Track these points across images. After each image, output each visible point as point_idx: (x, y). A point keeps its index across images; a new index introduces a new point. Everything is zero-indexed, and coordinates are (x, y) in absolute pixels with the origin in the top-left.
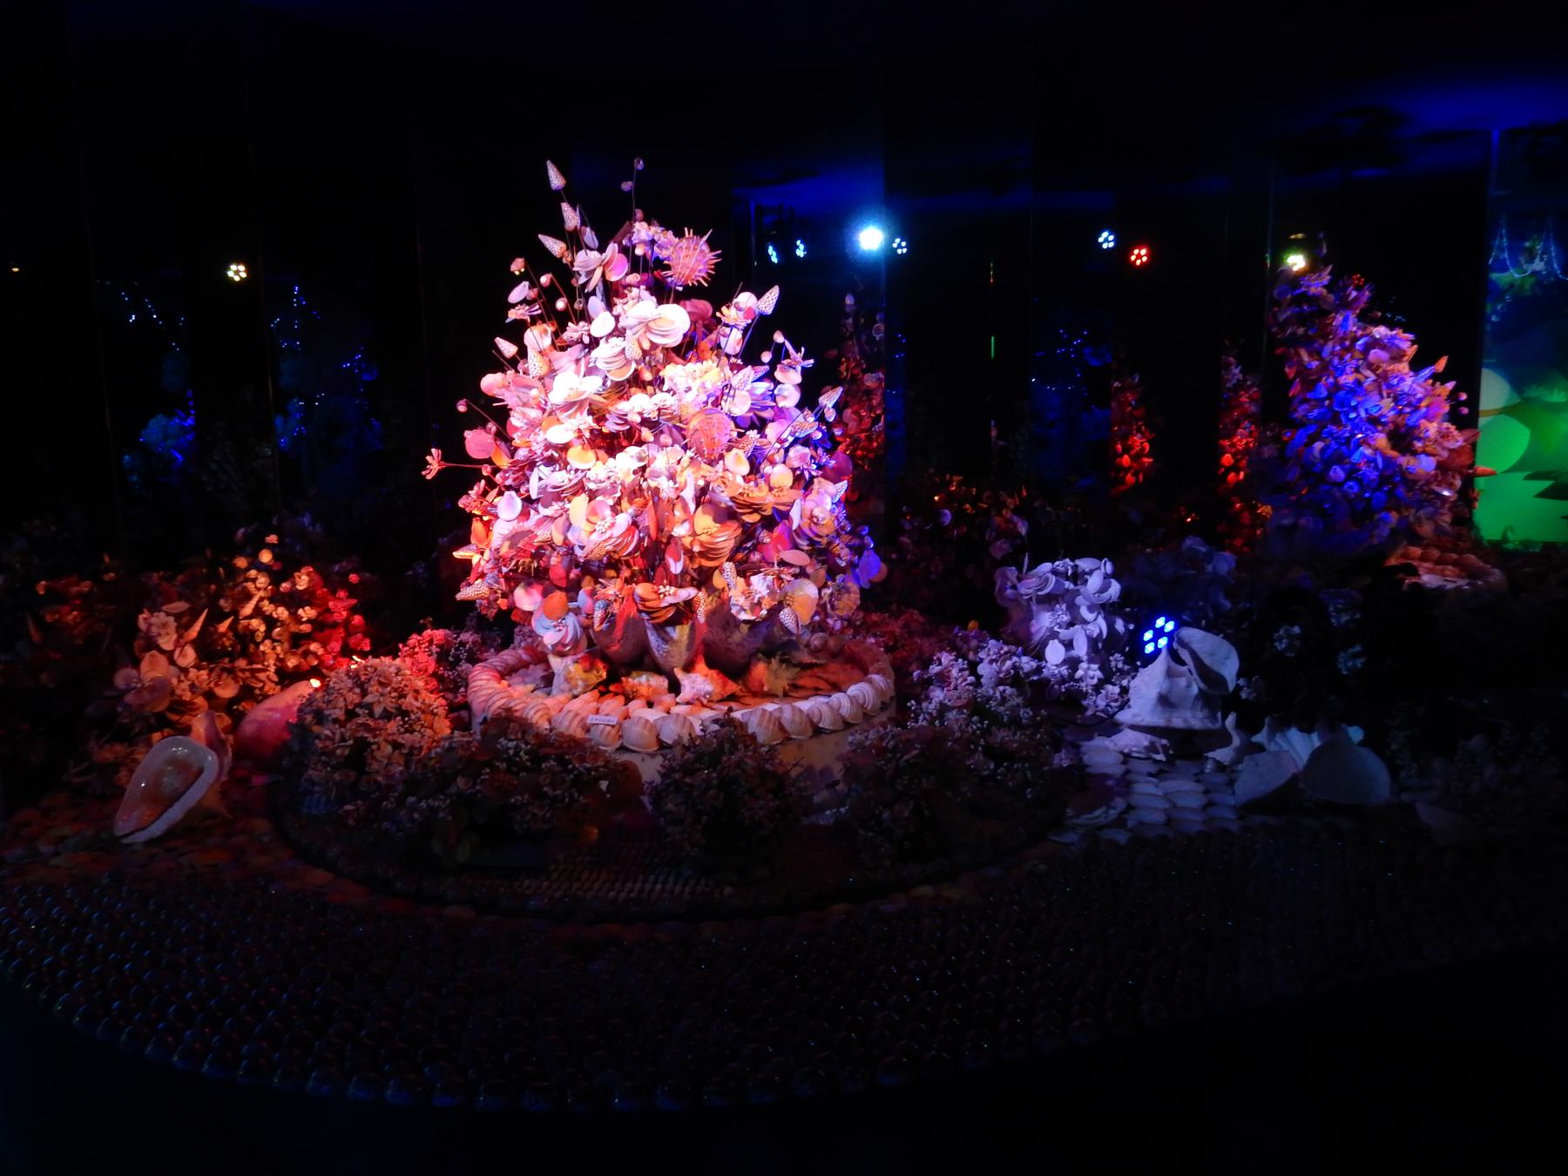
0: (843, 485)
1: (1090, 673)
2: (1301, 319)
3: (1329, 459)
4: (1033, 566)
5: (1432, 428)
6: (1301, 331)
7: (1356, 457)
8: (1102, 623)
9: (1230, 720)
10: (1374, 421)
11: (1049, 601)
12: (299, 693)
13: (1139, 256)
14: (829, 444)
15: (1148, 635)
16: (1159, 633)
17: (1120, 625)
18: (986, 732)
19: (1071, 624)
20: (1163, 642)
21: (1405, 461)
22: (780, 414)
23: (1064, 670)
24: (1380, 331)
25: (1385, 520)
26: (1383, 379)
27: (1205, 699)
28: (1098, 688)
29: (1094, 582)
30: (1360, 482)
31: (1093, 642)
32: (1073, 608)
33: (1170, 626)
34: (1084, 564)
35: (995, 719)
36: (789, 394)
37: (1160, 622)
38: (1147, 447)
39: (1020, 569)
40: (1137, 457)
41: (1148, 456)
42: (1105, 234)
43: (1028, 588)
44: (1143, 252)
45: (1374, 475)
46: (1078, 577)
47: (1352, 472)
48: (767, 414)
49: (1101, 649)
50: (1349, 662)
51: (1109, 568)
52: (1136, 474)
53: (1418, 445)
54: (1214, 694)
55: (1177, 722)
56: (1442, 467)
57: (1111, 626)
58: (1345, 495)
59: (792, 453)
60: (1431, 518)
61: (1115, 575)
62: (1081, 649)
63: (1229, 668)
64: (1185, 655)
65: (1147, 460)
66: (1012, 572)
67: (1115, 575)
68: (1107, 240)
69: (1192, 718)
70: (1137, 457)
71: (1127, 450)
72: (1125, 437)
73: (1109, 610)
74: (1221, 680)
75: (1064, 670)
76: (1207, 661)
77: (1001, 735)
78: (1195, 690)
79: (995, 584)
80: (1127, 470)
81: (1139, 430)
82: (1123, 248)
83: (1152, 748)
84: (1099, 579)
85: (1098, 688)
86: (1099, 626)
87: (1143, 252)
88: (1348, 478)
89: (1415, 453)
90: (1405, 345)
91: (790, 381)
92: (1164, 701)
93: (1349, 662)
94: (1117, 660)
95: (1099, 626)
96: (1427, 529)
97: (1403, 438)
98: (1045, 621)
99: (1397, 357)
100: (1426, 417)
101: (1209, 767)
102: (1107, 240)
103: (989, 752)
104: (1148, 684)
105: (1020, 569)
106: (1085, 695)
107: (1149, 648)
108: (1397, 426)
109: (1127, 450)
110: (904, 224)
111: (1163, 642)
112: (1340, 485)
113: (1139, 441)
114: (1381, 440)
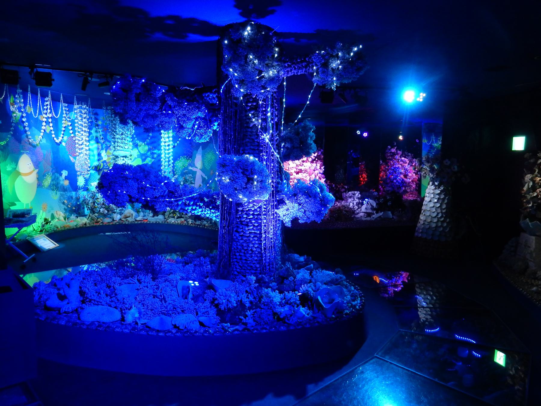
1: (356, 207)
2: (391, 156)
3: (394, 179)
4: (348, 192)
5: (410, 175)
8: (358, 200)
9: (375, 212)
10: (401, 173)
11: (350, 197)
12: (324, 183)
14: (322, 174)
15: (364, 201)
16: (366, 201)
17: (360, 201)
18: (345, 209)
20: (366, 202)
21: (405, 179)
22: (317, 169)
23: (352, 207)
25: (402, 189)
26: (403, 166)
27: (371, 209)
28: (357, 210)
29: (357, 195)
30: (398, 183)
31: (357, 203)
32: (354, 198)
34: (356, 192)
35: (346, 207)
36: (318, 167)
39: (346, 193)
40: (364, 179)
43: (347, 195)
45: (400, 182)
46: (354, 194)
47: (397, 181)
50: (389, 203)
51: (359, 193)
52: (364, 182)
53: (408, 177)
54: (373, 208)
55: (368, 211)
56: (412, 181)
58: (396, 185)
60: (410, 189)
61: (360, 194)
62: (355, 204)
63: (375, 205)
64: (369, 203)
65: (366, 179)
66: (345, 193)
69: (370, 211)
70: (364, 179)
71: (362, 177)
72: (362, 174)
73: (359, 198)
74: (374, 207)
75: (352, 207)
77: (346, 209)
78: (370, 207)
79: (225, 323)
80: (362, 181)
81: (364, 173)
83: (364, 215)
84: (357, 194)
85: (357, 210)
88: (396, 182)
89: (407, 178)
90: (407, 161)
91: (319, 165)
92: (366, 208)
96: (409, 190)
97: (406, 176)
98: (350, 200)
99: (406, 163)
100: (409, 173)
101: (372, 217)
102: (358, 132)
103: (345, 211)
105: (346, 193)
106: (355, 211)
108: (405, 174)
109: (362, 177)
110: (225, 40)
111: (366, 202)
112: (395, 183)
113: (364, 175)
114: (402, 176)
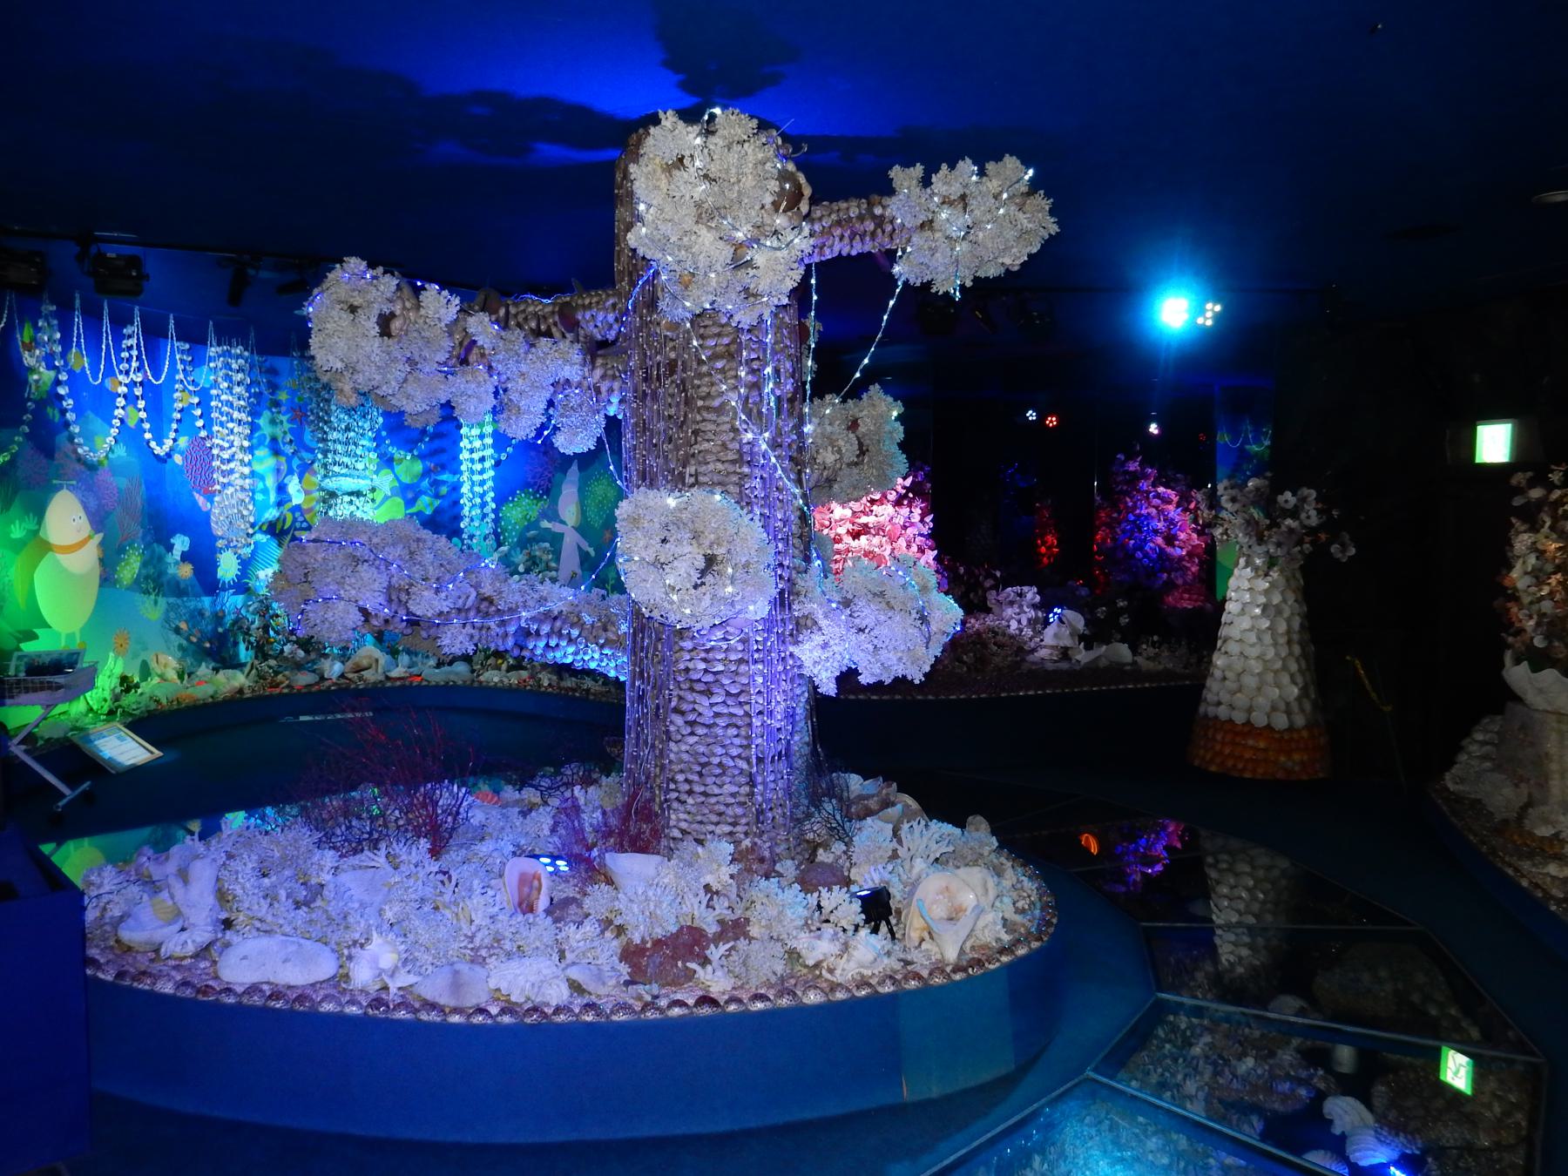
0: (936, 552)
1: (1028, 632)
4: (1003, 589)
5: (1182, 536)
6: (1125, 488)
7: (1147, 548)
10: (1156, 532)
13: (1051, 421)
15: (1051, 615)
16: (1055, 614)
19: (1019, 614)
21: (1169, 550)
22: (912, 524)
23: (1017, 632)
24: (1161, 489)
26: (1160, 512)
28: (1031, 639)
29: (1029, 596)
32: (1021, 606)
33: (1059, 611)
34: (1025, 589)
36: (916, 518)
37: (1056, 610)
38: (1055, 542)
39: (997, 591)
40: (1049, 548)
41: (1056, 547)
42: (1030, 412)
44: (1054, 419)
47: (1146, 555)
48: (907, 524)
49: (1032, 622)
50: (1124, 620)
52: (1049, 558)
57: (1036, 614)
59: (472, 590)
61: (1038, 593)
62: (1024, 622)
67: (1038, 593)
68: (1031, 415)
70: (1049, 548)
71: (1044, 543)
72: (1042, 536)
75: (1017, 632)
76: (1073, 623)
80: (1043, 555)
82: (1042, 418)
84: (1031, 594)
85: (1031, 639)
86: (1032, 614)
87: (1054, 419)
89: (1174, 546)
92: (1056, 636)
93: (1124, 620)
94: (1039, 627)
95: (1032, 614)
96: (1180, 582)
97: (1170, 539)
99: (1169, 502)
100: (1179, 530)
104: (1050, 632)
105: (997, 591)
106: (1025, 643)
107: (1051, 620)
109: (1044, 543)
112: (1141, 560)
113: (1051, 539)
114: (1160, 540)
